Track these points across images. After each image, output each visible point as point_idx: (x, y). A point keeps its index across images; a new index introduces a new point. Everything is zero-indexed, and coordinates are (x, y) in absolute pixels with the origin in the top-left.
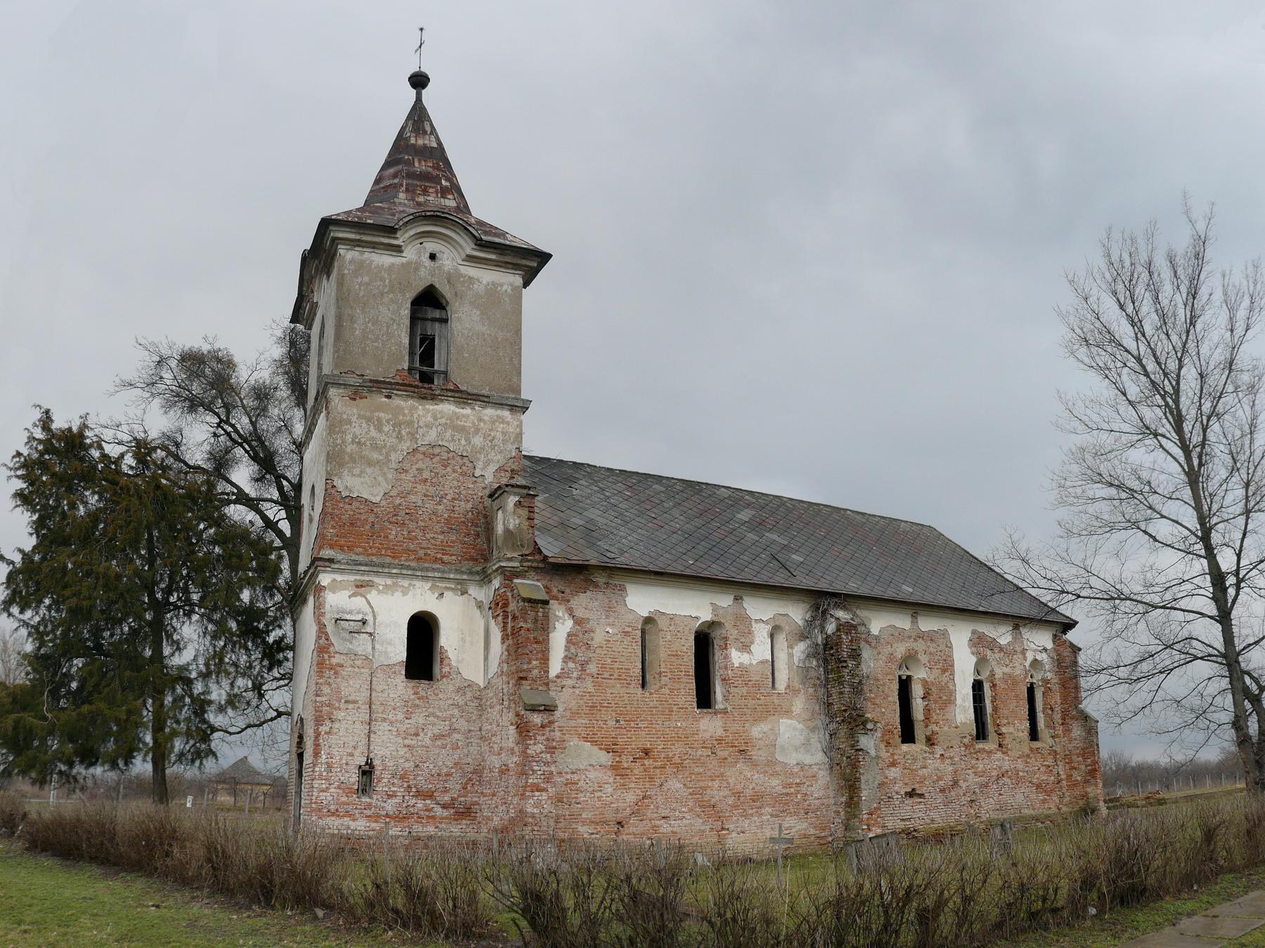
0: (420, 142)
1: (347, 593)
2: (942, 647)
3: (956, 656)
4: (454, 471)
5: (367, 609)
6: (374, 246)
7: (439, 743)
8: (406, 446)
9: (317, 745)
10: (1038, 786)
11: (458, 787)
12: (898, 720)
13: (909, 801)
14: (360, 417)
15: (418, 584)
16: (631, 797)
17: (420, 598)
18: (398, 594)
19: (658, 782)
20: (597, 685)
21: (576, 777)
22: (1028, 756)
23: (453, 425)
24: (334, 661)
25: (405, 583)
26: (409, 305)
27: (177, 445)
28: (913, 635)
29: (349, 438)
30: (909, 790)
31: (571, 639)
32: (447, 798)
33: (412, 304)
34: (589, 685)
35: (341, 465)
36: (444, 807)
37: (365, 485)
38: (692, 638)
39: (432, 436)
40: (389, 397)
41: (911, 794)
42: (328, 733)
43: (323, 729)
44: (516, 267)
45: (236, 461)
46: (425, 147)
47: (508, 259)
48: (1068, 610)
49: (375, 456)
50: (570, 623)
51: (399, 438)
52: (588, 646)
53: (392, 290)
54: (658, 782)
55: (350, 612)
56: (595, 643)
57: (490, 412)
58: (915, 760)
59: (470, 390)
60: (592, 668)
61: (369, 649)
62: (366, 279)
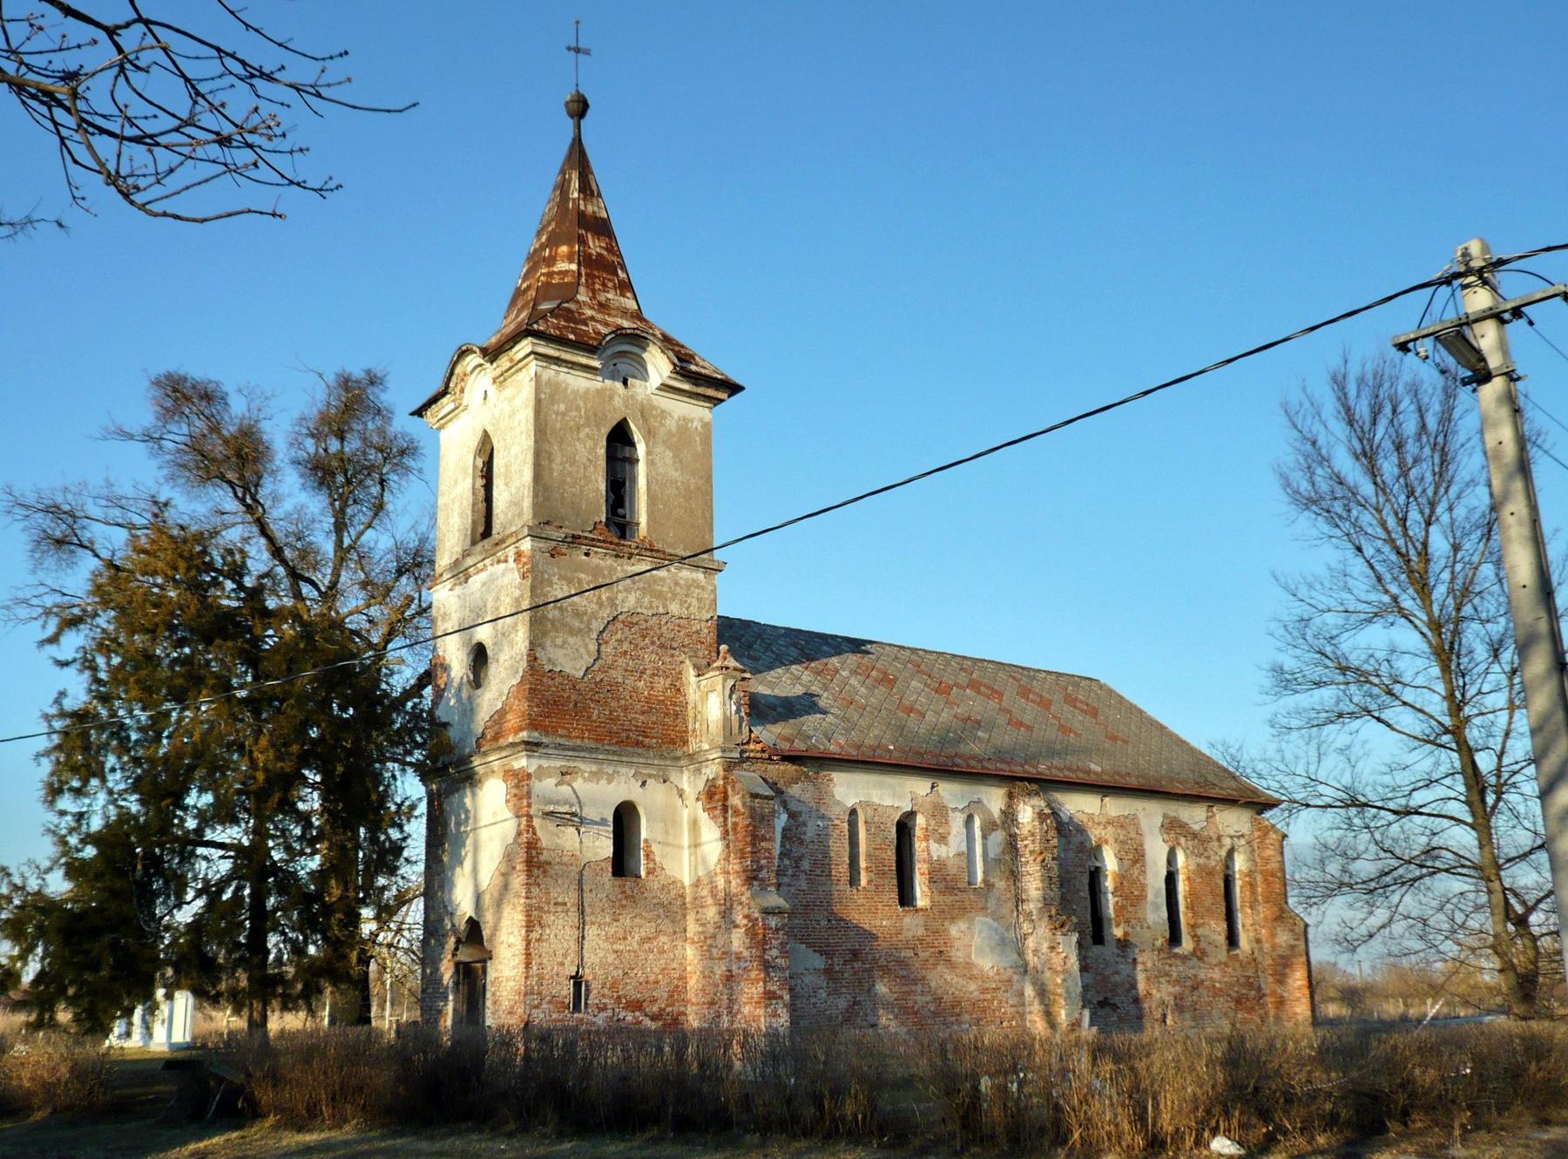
0: (590, 209)
2: (1133, 835)
3: (1147, 847)
4: (653, 643)
7: (646, 946)
8: (606, 614)
11: (665, 995)
14: (561, 578)
15: (623, 770)
16: (842, 1003)
22: (1226, 965)
24: (542, 858)
26: (604, 443)
28: (1103, 820)
30: (1101, 998)
31: (787, 834)
32: (655, 1009)
36: (652, 1019)
37: (571, 658)
40: (587, 554)
42: (538, 940)
43: (534, 935)
47: (700, 390)
51: (600, 604)
52: (801, 843)
58: (1107, 964)
60: (805, 865)
61: (577, 845)
62: (562, 407)
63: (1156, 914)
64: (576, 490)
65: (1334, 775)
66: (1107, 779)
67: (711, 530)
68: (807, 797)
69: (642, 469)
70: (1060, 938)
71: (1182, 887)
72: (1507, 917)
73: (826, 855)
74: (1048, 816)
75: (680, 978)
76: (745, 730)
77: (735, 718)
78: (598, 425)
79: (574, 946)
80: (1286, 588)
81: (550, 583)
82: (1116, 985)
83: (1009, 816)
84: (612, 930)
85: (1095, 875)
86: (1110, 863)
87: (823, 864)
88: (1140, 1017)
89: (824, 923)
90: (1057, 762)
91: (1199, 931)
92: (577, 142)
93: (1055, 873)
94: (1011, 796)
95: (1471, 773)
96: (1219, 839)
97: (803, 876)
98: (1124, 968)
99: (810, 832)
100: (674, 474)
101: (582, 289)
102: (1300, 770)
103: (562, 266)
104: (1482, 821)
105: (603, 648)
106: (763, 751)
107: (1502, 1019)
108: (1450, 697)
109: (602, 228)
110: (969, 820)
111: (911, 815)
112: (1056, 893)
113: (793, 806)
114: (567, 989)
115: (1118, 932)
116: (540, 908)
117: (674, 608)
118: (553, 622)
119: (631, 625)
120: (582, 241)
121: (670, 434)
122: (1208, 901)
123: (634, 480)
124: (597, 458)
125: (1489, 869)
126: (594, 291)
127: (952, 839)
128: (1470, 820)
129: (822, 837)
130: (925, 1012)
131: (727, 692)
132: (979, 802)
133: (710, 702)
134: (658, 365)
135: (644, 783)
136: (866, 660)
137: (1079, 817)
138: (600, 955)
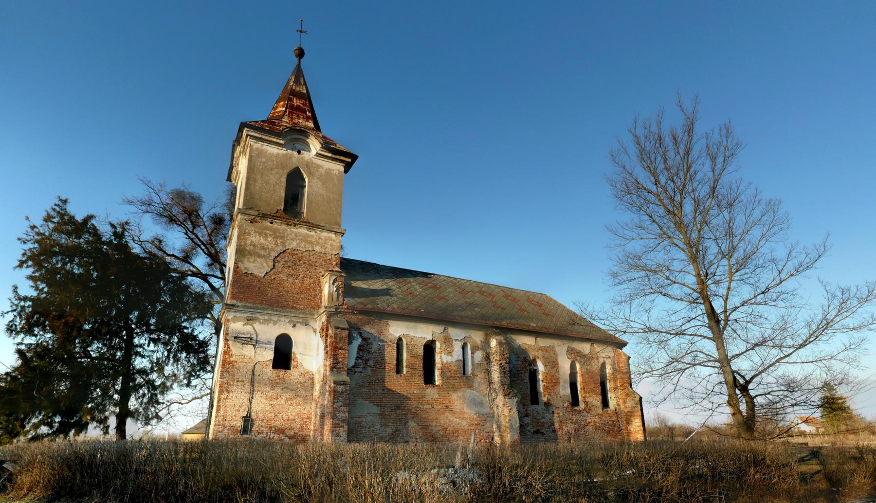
0: (298, 89)
1: (242, 323)
2: (552, 355)
5: (253, 332)
7: (289, 402)
8: (280, 249)
9: (218, 406)
10: (608, 432)
11: (298, 426)
13: (536, 436)
14: (255, 232)
15: (283, 319)
16: (389, 431)
17: (282, 327)
18: (271, 324)
20: (373, 371)
21: (360, 420)
23: (305, 239)
24: (232, 359)
27: (160, 241)
29: (249, 242)
30: (535, 429)
31: (360, 348)
32: (292, 433)
34: (369, 371)
35: (244, 256)
36: (290, 438)
37: (258, 268)
38: (422, 348)
39: (294, 245)
40: (271, 223)
41: (537, 432)
43: (223, 396)
45: (197, 254)
46: (299, 92)
48: (624, 338)
49: (263, 252)
50: (360, 340)
51: (277, 245)
52: (369, 352)
53: (277, 167)
55: (243, 333)
57: (325, 234)
60: (371, 363)
61: (253, 353)
62: (264, 160)
65: (640, 320)
68: (373, 331)
70: (508, 400)
73: (383, 359)
74: (504, 344)
75: (308, 418)
76: (341, 299)
77: (335, 294)
78: (283, 170)
79: (246, 402)
80: (611, 231)
82: (543, 423)
83: (486, 343)
85: (534, 374)
86: (541, 367)
87: (381, 363)
88: (556, 439)
89: (380, 391)
90: (513, 321)
91: (587, 400)
93: (507, 370)
94: (486, 335)
97: (369, 369)
98: (548, 416)
99: (375, 347)
100: (322, 192)
101: (285, 117)
102: (621, 316)
103: (279, 109)
104: (718, 337)
105: (277, 264)
106: (347, 308)
107: (150, 245)
108: (698, 275)
109: (307, 98)
110: (464, 348)
112: (507, 380)
113: (365, 335)
114: (239, 424)
115: (545, 399)
116: (228, 383)
117: (318, 249)
119: (293, 255)
121: (321, 175)
123: (303, 194)
125: (724, 362)
126: (292, 118)
127: (454, 354)
128: (711, 335)
129: (381, 350)
131: (332, 282)
132: (470, 337)
134: (315, 145)
135: (294, 326)
136: (428, 280)
137: (524, 346)
138: (262, 406)
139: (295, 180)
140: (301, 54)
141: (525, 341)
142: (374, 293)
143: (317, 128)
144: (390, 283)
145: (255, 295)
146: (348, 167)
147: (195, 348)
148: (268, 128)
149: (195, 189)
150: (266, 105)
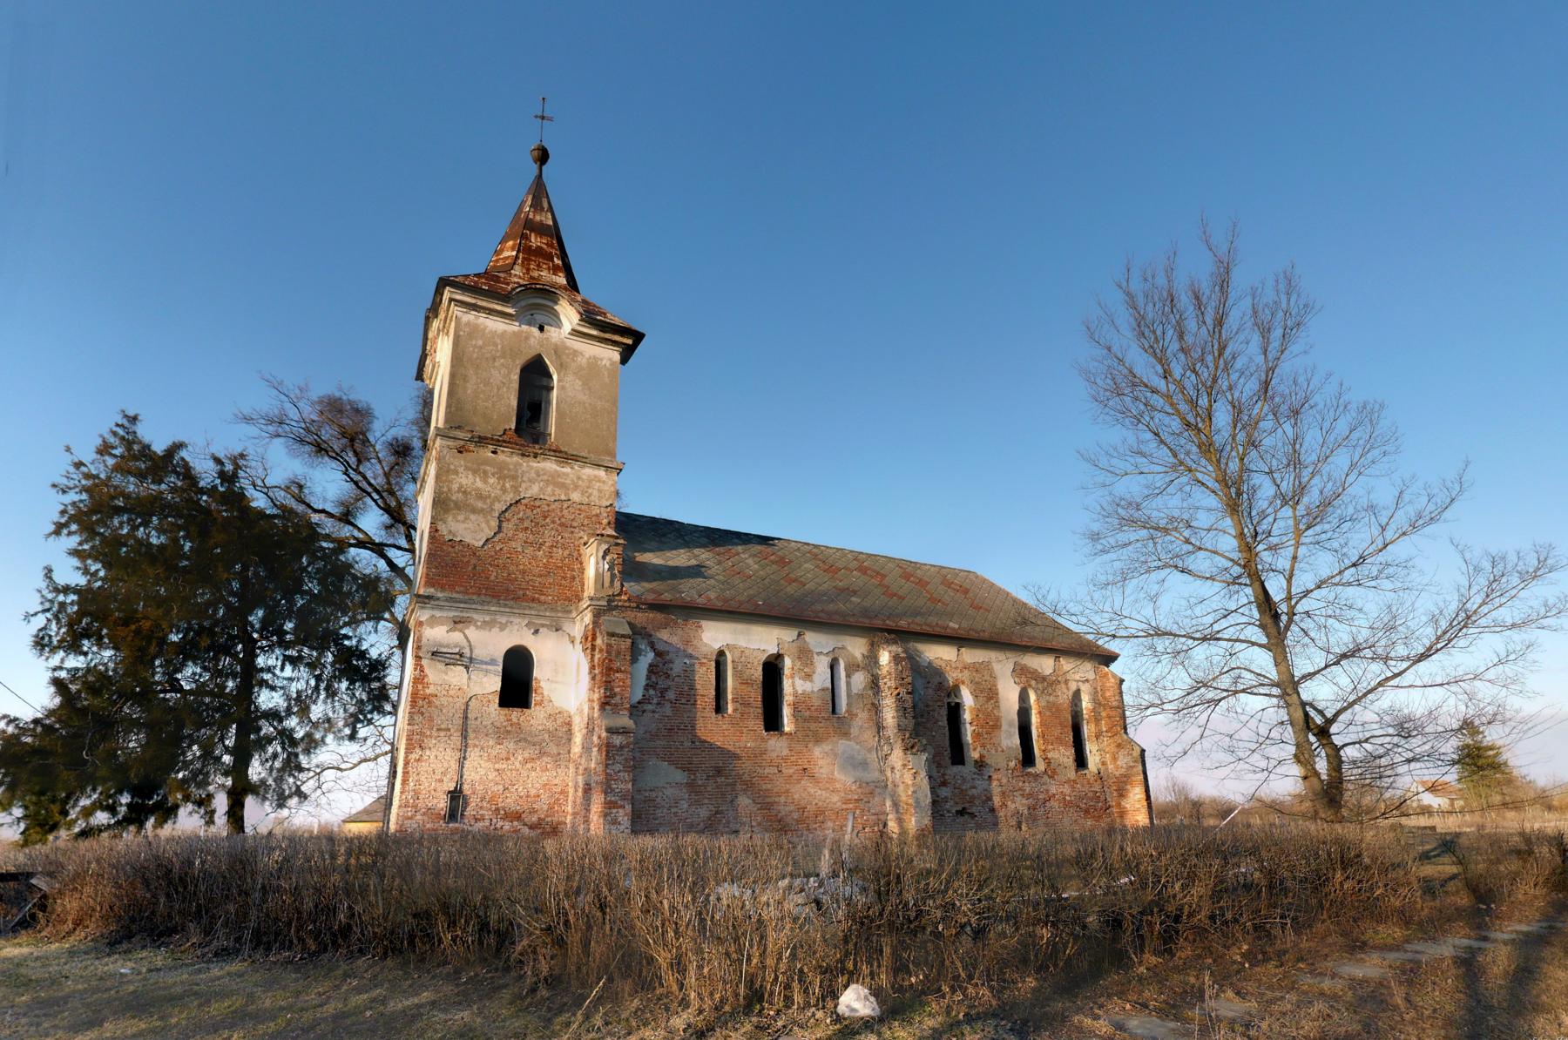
0: (538, 218)
2: (987, 677)
3: (1000, 687)
5: (465, 643)
6: (491, 312)
8: (510, 497)
9: (405, 773)
12: (947, 743)
13: (960, 820)
14: (467, 468)
15: (516, 620)
16: (704, 813)
17: (515, 634)
18: (496, 630)
19: (729, 798)
21: (654, 794)
23: (553, 480)
24: (428, 691)
25: (504, 620)
31: (652, 669)
32: (534, 819)
33: (523, 370)
34: (668, 710)
35: (447, 511)
36: (531, 828)
38: (760, 668)
39: (535, 490)
41: (962, 813)
43: (413, 757)
44: (615, 343)
48: (1113, 646)
49: (480, 504)
50: (651, 655)
52: (668, 676)
53: (503, 356)
54: (729, 798)
55: (448, 646)
56: (674, 673)
57: (588, 471)
58: (964, 779)
59: (571, 451)
60: (671, 695)
61: (465, 681)
62: (480, 343)
63: (1011, 740)
64: (489, 404)
66: (962, 633)
67: (615, 440)
68: (674, 640)
69: (555, 393)
70: (910, 757)
71: (1035, 720)
72: (1308, 728)
73: (692, 687)
76: (617, 584)
77: (607, 576)
79: (454, 766)
80: (1089, 460)
81: (456, 472)
82: (973, 797)
83: (872, 659)
84: (494, 753)
85: (955, 711)
86: (967, 698)
87: (688, 696)
88: (996, 824)
90: (918, 619)
92: (540, 176)
93: (909, 704)
95: (1265, 602)
96: (1066, 682)
97: (668, 705)
102: (1107, 608)
103: (506, 254)
109: (554, 233)
111: (779, 657)
112: (910, 723)
113: (660, 647)
114: (442, 803)
115: (975, 755)
116: (421, 733)
117: (575, 496)
118: (456, 503)
119: (533, 508)
120: (527, 238)
121: (581, 368)
122: (1057, 732)
123: (549, 402)
124: (510, 381)
125: (1288, 687)
127: (816, 677)
128: (1264, 640)
129: (689, 673)
130: (788, 820)
131: (601, 554)
132: (843, 648)
133: (593, 564)
134: (569, 316)
136: (770, 549)
137: (937, 663)
139: (535, 375)
140: (543, 156)
141: (939, 654)
142: (676, 573)
143: (573, 285)
144: (703, 555)
145: (467, 579)
146: (627, 354)
147: (363, 672)
148: (486, 288)
149: (361, 394)
150: (483, 245)
